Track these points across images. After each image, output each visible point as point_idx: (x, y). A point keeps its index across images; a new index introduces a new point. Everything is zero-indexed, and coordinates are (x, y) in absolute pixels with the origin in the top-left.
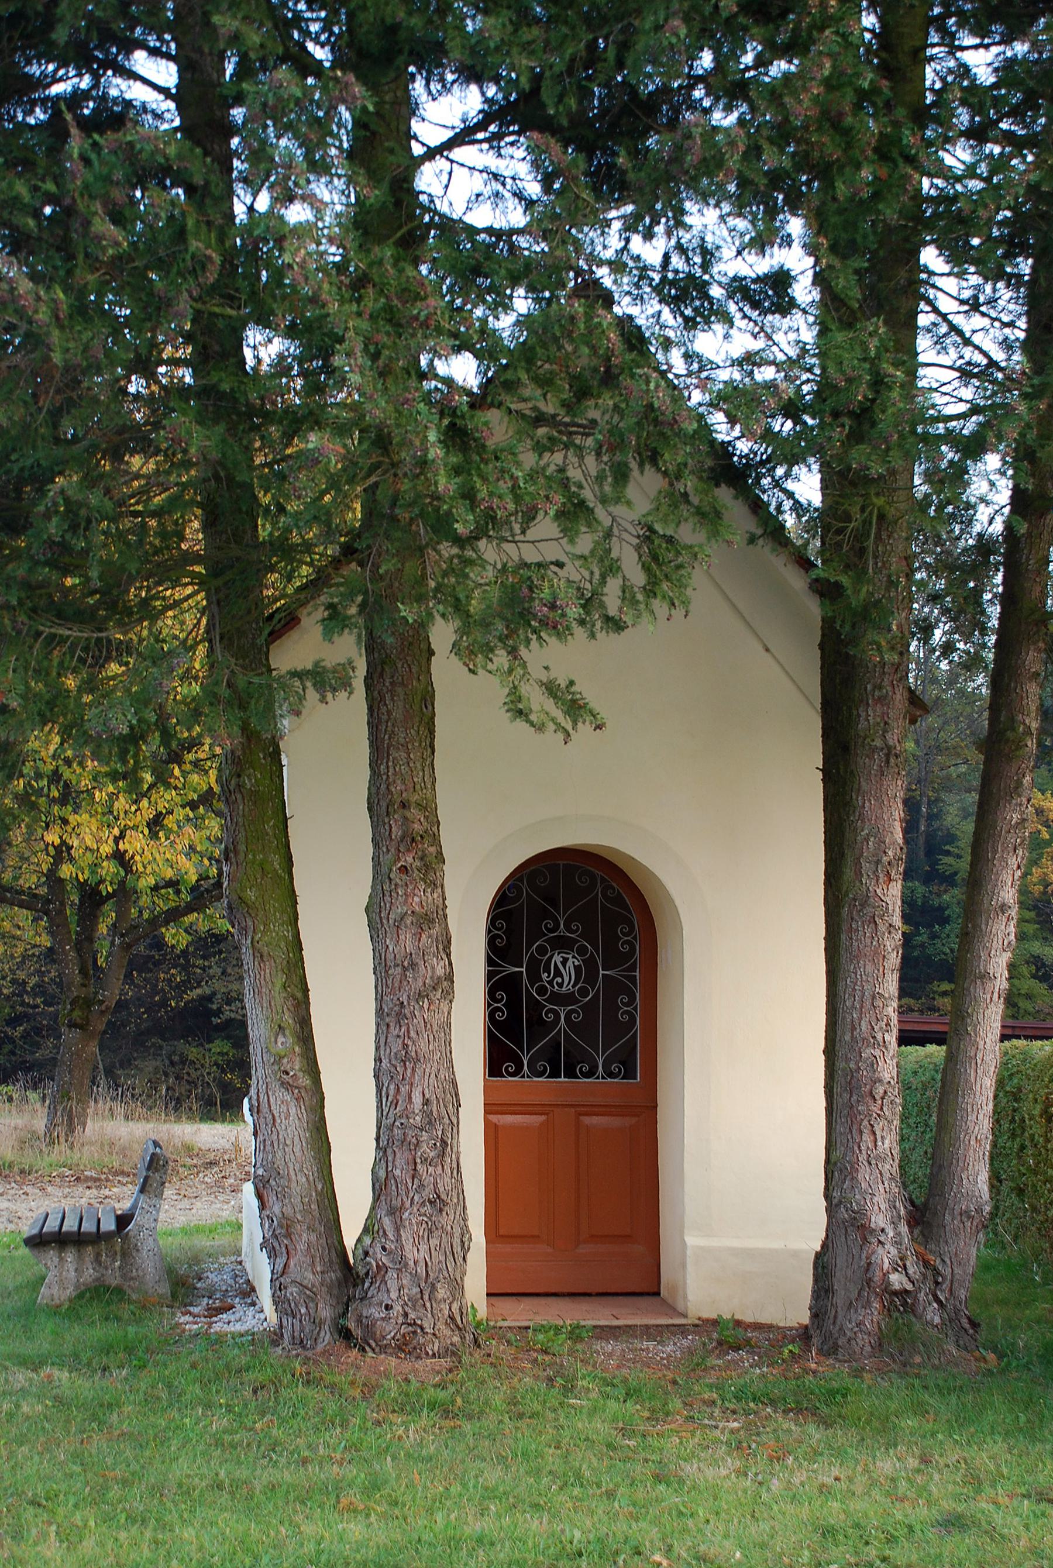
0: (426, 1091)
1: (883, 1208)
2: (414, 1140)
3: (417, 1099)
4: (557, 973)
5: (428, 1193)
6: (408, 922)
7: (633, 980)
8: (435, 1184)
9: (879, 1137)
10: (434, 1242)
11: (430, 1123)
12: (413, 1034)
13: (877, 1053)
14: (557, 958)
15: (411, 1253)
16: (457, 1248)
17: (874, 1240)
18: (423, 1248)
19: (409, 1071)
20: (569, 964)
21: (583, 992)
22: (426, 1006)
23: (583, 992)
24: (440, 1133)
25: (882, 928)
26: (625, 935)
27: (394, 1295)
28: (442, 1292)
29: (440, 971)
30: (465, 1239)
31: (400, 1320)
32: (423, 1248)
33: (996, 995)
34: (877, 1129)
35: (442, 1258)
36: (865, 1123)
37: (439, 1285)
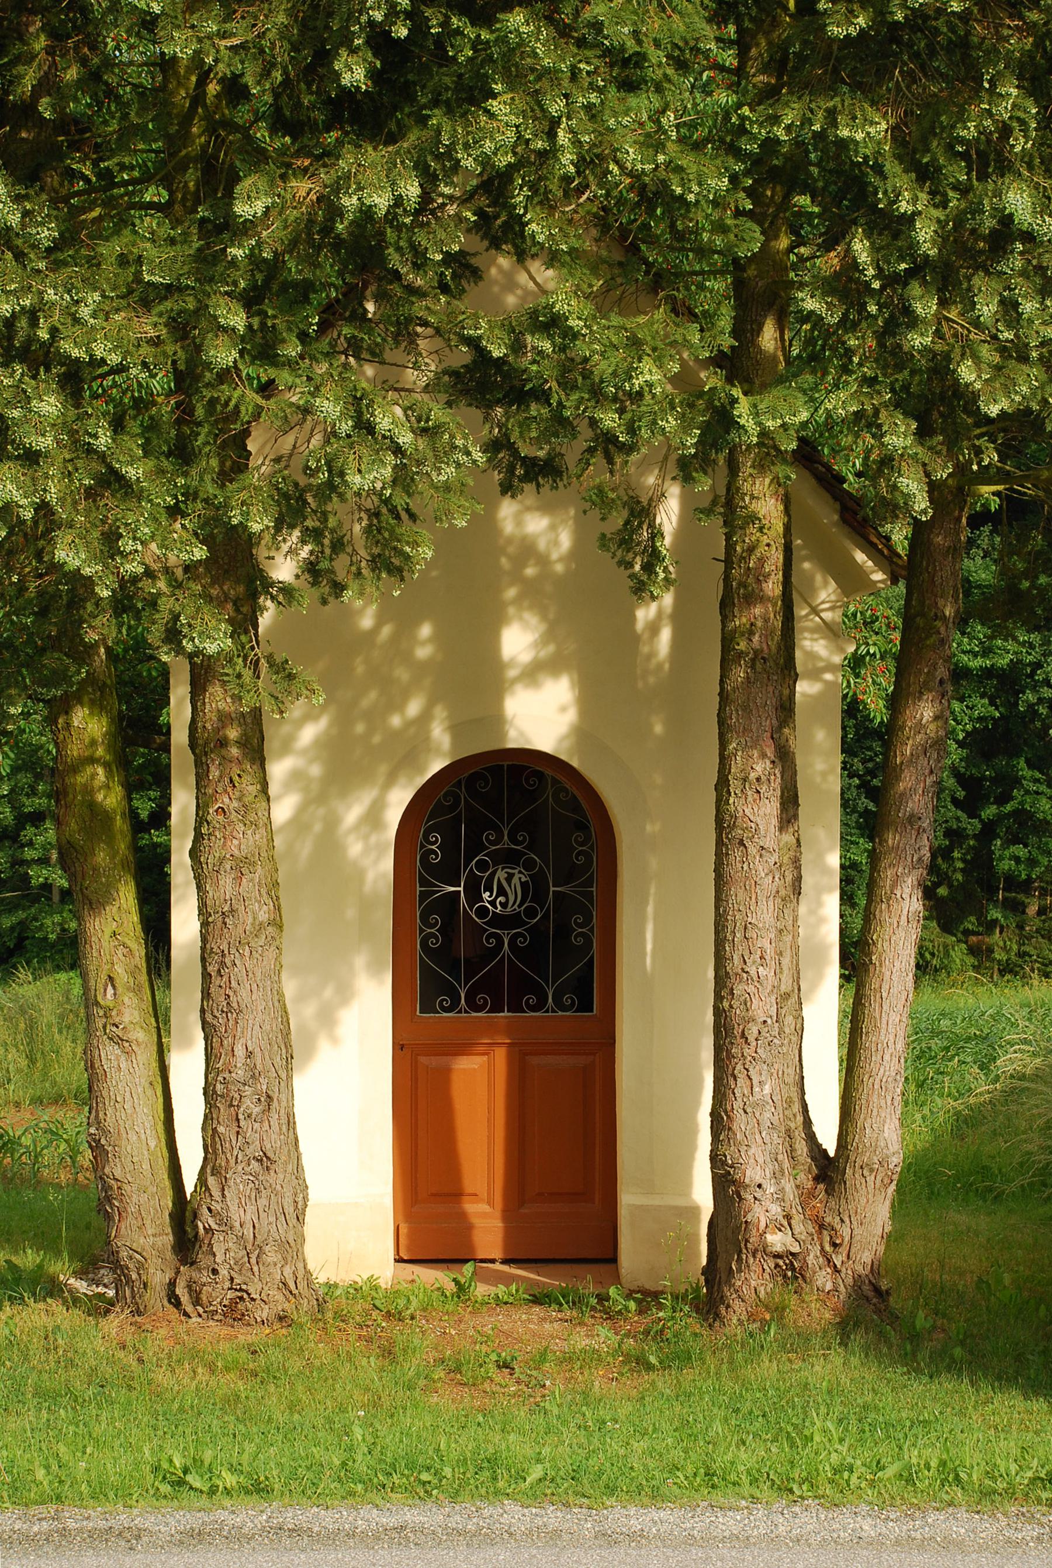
0: (249, 1044)
1: (761, 1160)
2: (237, 1096)
3: (240, 1051)
4: (502, 892)
5: (254, 1150)
6: (228, 867)
7: (589, 896)
8: (262, 1140)
9: (755, 1082)
10: (263, 1202)
11: (253, 1077)
12: (234, 984)
13: (751, 989)
14: (501, 875)
15: (236, 1215)
16: (290, 1209)
17: (750, 1198)
18: (251, 1209)
19: (231, 1022)
20: (515, 880)
21: (531, 913)
22: (247, 953)
23: (531, 913)
24: (264, 1087)
25: (752, 850)
26: (582, 844)
27: (219, 1259)
28: (271, 1256)
29: (263, 916)
30: (300, 1199)
31: (227, 1284)
32: (251, 1209)
33: (904, 918)
34: (752, 1073)
35: (272, 1219)
36: (739, 1067)
37: (267, 1249)
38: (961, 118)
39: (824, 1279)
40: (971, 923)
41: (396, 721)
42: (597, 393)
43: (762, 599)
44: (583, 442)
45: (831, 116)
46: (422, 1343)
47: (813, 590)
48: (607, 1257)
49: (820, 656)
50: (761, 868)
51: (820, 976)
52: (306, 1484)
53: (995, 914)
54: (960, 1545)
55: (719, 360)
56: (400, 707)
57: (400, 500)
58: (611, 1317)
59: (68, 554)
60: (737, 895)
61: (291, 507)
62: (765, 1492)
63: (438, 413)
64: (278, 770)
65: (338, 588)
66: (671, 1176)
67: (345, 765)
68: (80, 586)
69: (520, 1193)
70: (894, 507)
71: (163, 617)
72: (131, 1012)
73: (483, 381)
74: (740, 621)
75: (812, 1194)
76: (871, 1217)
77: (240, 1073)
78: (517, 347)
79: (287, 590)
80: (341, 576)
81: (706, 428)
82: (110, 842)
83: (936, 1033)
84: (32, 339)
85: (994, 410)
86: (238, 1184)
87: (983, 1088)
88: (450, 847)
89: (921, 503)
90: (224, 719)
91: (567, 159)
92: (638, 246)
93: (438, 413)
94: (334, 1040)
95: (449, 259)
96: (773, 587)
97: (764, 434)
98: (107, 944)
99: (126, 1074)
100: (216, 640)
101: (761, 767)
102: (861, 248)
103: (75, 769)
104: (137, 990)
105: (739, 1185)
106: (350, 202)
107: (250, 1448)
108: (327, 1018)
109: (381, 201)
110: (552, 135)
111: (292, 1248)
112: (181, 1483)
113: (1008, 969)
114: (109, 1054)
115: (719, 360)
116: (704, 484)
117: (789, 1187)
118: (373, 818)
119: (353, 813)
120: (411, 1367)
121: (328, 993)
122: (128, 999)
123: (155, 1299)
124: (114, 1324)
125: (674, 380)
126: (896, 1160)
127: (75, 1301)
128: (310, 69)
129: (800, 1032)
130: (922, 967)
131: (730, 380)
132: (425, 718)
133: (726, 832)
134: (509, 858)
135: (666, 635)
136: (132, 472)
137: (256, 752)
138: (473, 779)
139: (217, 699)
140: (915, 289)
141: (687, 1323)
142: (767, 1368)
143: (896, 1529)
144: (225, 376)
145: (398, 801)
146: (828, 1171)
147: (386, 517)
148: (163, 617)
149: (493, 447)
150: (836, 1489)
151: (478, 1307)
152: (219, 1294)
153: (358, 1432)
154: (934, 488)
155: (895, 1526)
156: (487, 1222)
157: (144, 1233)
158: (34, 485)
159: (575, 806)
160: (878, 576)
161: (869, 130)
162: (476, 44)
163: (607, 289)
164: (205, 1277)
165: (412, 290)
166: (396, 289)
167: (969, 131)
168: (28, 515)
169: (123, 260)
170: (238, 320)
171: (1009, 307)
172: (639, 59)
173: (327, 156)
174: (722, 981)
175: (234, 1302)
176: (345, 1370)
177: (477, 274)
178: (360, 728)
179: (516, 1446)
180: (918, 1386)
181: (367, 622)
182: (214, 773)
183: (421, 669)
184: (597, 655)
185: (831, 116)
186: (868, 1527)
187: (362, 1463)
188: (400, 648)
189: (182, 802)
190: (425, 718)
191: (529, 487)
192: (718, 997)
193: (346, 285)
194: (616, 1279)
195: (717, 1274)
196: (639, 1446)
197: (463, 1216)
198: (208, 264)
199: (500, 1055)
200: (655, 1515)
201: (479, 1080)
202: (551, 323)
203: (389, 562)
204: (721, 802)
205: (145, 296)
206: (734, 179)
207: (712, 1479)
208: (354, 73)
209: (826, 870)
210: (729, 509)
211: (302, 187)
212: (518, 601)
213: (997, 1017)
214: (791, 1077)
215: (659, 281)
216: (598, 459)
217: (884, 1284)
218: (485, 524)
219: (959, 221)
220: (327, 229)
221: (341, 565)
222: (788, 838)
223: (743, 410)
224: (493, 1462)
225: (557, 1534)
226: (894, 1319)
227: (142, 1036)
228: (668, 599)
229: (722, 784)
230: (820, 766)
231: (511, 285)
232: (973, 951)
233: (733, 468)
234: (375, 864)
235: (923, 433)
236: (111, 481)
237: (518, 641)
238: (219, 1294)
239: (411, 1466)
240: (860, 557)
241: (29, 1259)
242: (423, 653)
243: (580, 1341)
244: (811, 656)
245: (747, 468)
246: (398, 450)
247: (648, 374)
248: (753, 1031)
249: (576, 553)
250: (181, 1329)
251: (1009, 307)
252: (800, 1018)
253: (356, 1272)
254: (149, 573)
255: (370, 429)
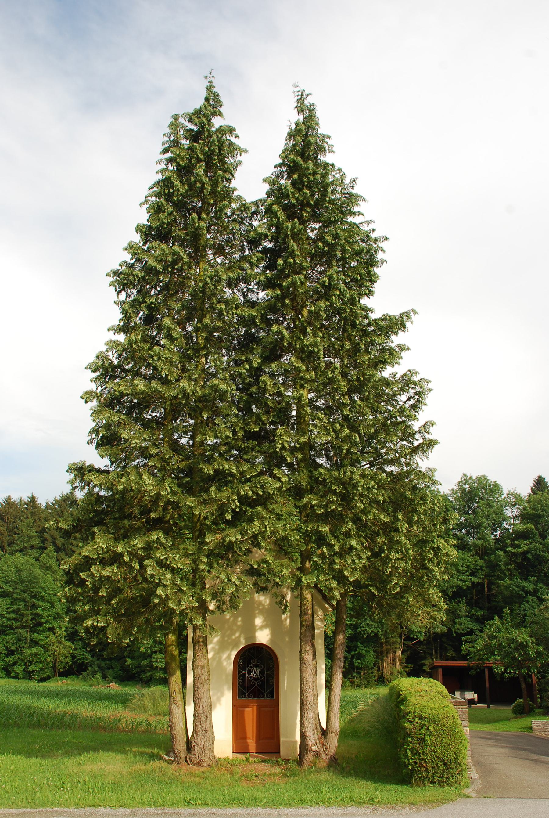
14: (255, 669)
15: (200, 742)
21: (261, 677)
23: (261, 677)
28: (207, 752)
29: (206, 678)
38: (342, 527)
39: (324, 756)
40: (350, 676)
41: (233, 637)
42: (275, 575)
43: (308, 614)
44: (272, 584)
45: (318, 526)
46: (239, 770)
47: (317, 612)
48: (277, 752)
49: (320, 627)
50: (309, 669)
51: (321, 691)
52: (216, 803)
53: (355, 674)
54: (354, 814)
55: (298, 569)
56: (234, 634)
57: (236, 595)
58: (279, 765)
59: (171, 605)
60: (304, 674)
61: (215, 596)
62: (313, 804)
63: (244, 578)
64: (210, 647)
65: (224, 611)
66: (291, 734)
67: (223, 646)
68: (174, 611)
69: (259, 738)
70: (333, 598)
71: (189, 617)
72: (179, 698)
73: (252, 572)
74: (304, 618)
75: (321, 738)
76: (333, 742)
77: (201, 712)
78: (259, 565)
79: (213, 611)
80: (224, 609)
81: (296, 582)
82: (175, 662)
83: (344, 701)
84: (166, 563)
85: (351, 580)
86: (200, 735)
87: (355, 714)
88: (244, 663)
89: (339, 597)
90: (199, 637)
91: (269, 532)
92: (282, 547)
93: (244, 578)
94: (220, 704)
95: (246, 549)
96: (310, 612)
97: (308, 583)
98: (174, 683)
99: (177, 711)
100: (199, 622)
101: (308, 648)
102: (325, 550)
103: (169, 646)
104: (180, 693)
105: (306, 736)
106: (227, 539)
107: (203, 795)
108: (219, 700)
109: (233, 539)
110: (266, 528)
111: (211, 750)
112: (189, 802)
113: (358, 686)
114: (174, 707)
115: (298, 569)
116: (296, 593)
117: (316, 736)
118: (229, 657)
119: (225, 656)
120: (237, 777)
121: (219, 694)
122: (178, 695)
123: (182, 761)
124: (174, 766)
125: (290, 572)
126: (338, 730)
127: (165, 761)
128: (220, 515)
129: (318, 703)
130: (342, 687)
131: (301, 573)
132: (239, 636)
133: (302, 661)
134: (256, 666)
135: (288, 620)
136: (184, 589)
137: (205, 644)
138: (249, 649)
139: (198, 633)
140: (335, 557)
141: (295, 766)
142: (313, 776)
143: (341, 812)
144: (202, 570)
145: (234, 654)
146: (324, 733)
147: (233, 598)
148: (189, 617)
149: (254, 584)
150: (328, 803)
151: (250, 763)
152: (196, 760)
153: (226, 792)
154: (341, 594)
155: (341, 811)
156: (252, 744)
157: (180, 746)
158: (165, 591)
159: (270, 655)
160: (330, 609)
161: (325, 529)
162: (251, 512)
163: (276, 555)
164: (193, 756)
165: (238, 555)
166: (236, 555)
167: (344, 530)
168: (164, 597)
169: (184, 549)
170: (206, 560)
171: (353, 561)
172: (282, 515)
173: (223, 530)
174: (302, 692)
175: (199, 762)
176: (223, 777)
177: (251, 552)
178: (226, 639)
179: (260, 795)
180: (344, 780)
181: (228, 617)
182: (197, 648)
183: (239, 627)
184: (274, 624)
185: (318, 526)
186: (335, 811)
187: (227, 799)
188: (235, 622)
189: (190, 653)
190: (239, 636)
191: (261, 592)
192: (301, 696)
193: (225, 553)
194: (280, 757)
195: (301, 755)
196: (286, 794)
197: (247, 742)
198: (200, 550)
199: (255, 708)
200: (290, 810)
201: (250, 713)
202: (266, 562)
203: (234, 606)
204: (300, 655)
205: (187, 555)
206: (300, 536)
207: (302, 802)
208: (229, 517)
209: (322, 669)
210: (301, 597)
211: (218, 536)
212: (258, 613)
213: (356, 697)
214: (316, 713)
215: (287, 553)
216: (275, 587)
217: (336, 757)
218: (252, 599)
219: (343, 545)
220: (223, 544)
221: (224, 607)
222: (314, 662)
223: (303, 579)
224: (255, 798)
225: (269, 815)
226: (339, 765)
227: (181, 703)
228: (289, 614)
229: (301, 651)
230: (320, 647)
231: (257, 553)
232: (351, 682)
233: (301, 589)
234: (229, 667)
235: (338, 584)
236: (180, 590)
237: (258, 621)
238: (196, 760)
239: (238, 799)
240: (326, 605)
241: (156, 751)
242: (239, 623)
243: (273, 771)
244: (317, 625)
245: (304, 588)
246: (236, 585)
247: (285, 571)
248: (308, 703)
249: (270, 604)
250: (188, 768)
251: (353, 561)
252: (317, 700)
253: (225, 756)
254: (187, 608)
255: (231, 581)
